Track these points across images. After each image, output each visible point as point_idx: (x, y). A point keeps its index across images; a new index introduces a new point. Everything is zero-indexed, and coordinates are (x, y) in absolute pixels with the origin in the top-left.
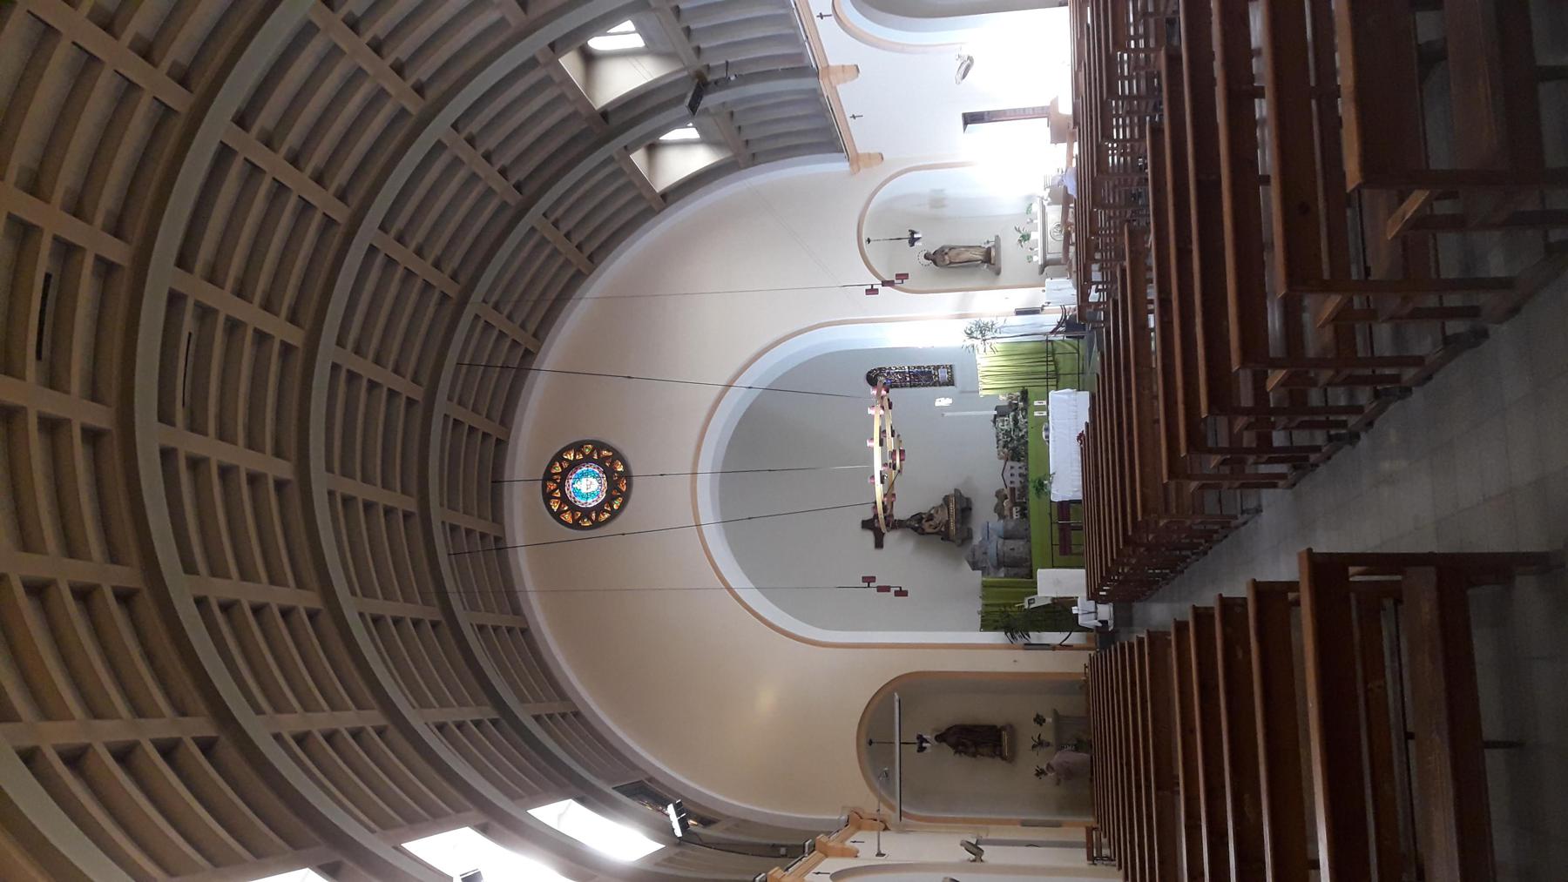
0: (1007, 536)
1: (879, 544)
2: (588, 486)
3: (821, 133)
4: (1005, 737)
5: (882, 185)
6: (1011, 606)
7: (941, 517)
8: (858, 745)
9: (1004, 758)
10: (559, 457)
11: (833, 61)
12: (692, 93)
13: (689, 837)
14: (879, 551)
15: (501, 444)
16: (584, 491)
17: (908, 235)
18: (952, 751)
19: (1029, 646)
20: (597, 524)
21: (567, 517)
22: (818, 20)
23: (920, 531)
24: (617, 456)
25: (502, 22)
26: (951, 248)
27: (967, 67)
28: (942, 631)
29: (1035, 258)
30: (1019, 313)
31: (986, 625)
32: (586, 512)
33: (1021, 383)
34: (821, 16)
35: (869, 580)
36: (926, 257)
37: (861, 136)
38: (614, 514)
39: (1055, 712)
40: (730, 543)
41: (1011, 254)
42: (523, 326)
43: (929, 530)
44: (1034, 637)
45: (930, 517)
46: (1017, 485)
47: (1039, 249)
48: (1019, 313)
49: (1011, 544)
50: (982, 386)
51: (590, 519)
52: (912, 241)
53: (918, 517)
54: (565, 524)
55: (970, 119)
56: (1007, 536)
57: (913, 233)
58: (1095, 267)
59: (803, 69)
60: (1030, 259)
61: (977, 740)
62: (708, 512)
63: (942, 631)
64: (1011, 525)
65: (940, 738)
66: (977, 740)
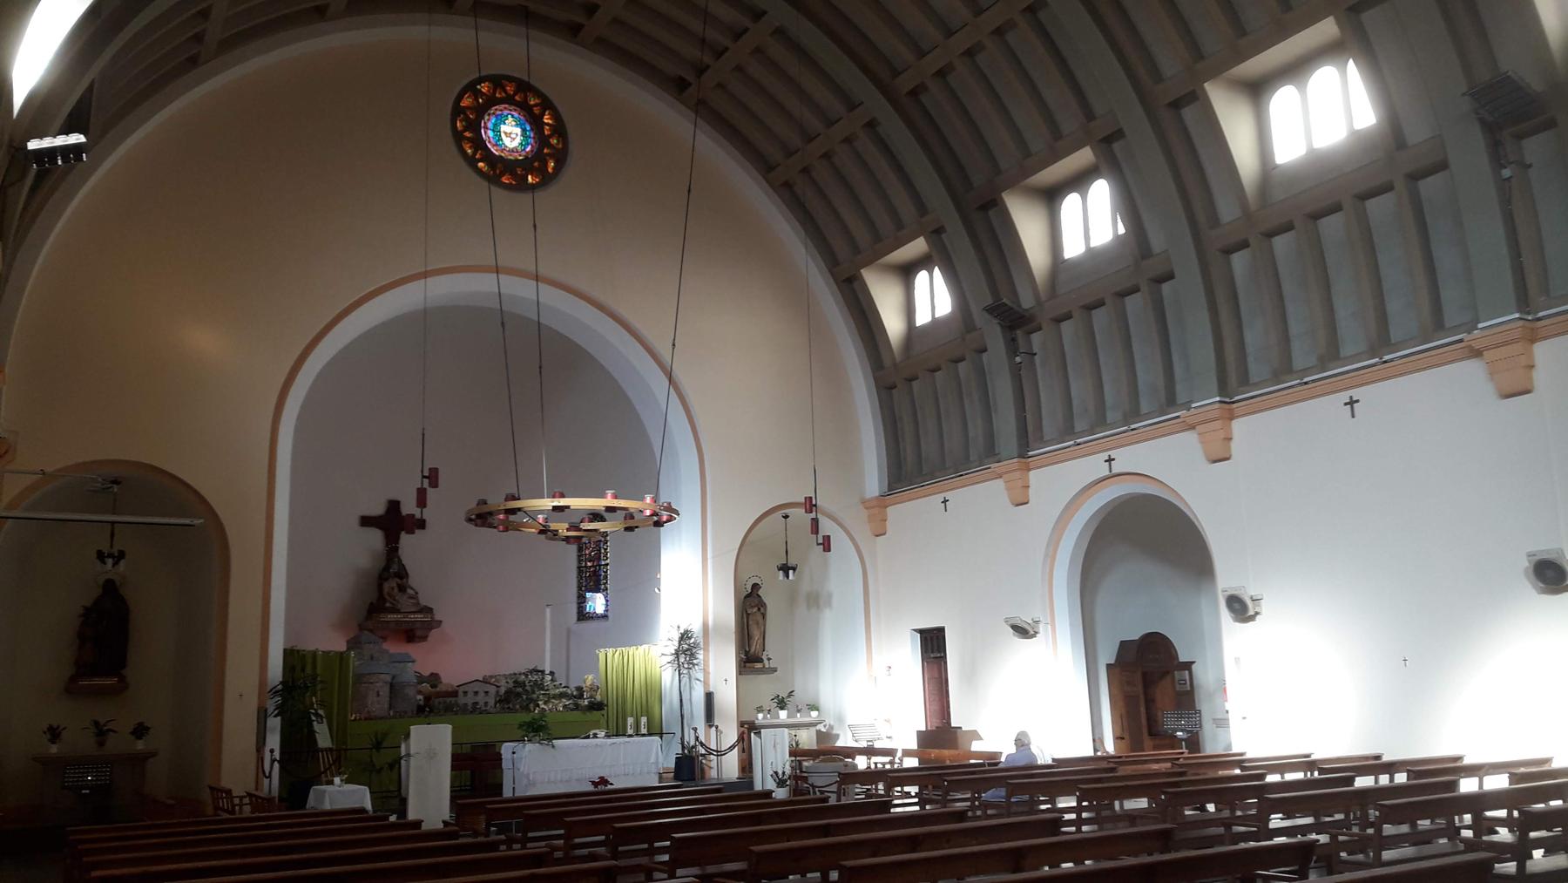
1: (366, 521)
2: (510, 135)
3: (914, 466)
5: (852, 539)
6: (314, 694)
7: (404, 602)
8: (101, 463)
9: (73, 679)
10: (547, 104)
12: (1007, 307)
13: (19, 153)
14: (355, 522)
15: (573, 31)
16: (503, 128)
17: (791, 563)
18: (88, 602)
19: (262, 715)
20: (458, 137)
21: (467, 101)
22: (1105, 456)
23: (383, 576)
24: (546, 180)
26: (764, 615)
27: (1022, 631)
28: (282, 599)
29: (760, 716)
30: (709, 697)
31: (290, 654)
32: (475, 126)
36: (755, 587)
37: (917, 512)
39: (153, 754)
40: (384, 324)
41: (765, 688)
43: (386, 586)
44: (275, 723)
45: (402, 589)
46: (462, 700)
48: (709, 697)
50: (610, 651)
52: (785, 569)
53: (402, 574)
54: (460, 97)
55: (933, 643)
57: (794, 569)
58: (1002, 792)
59: (1027, 443)
60: (760, 709)
61: (103, 640)
63: (282, 599)
64: (411, 692)
65: (110, 589)
66: (103, 640)
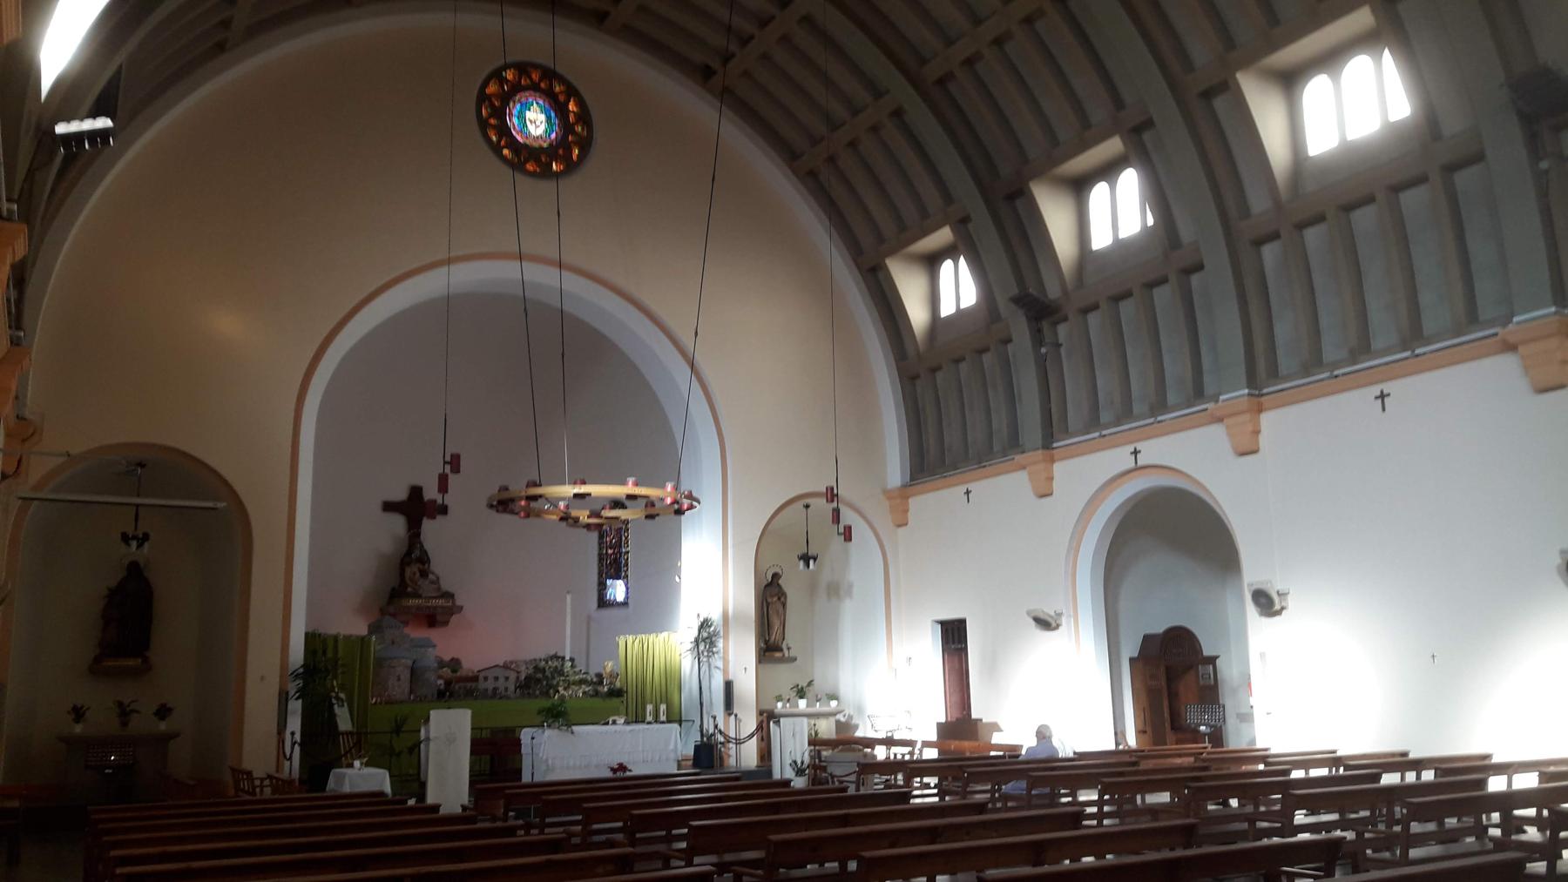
0: (415, 673)
1: (389, 507)
3: (935, 457)
4: (131, 662)
10: (572, 92)
11: (1058, 468)
12: (1034, 299)
16: (530, 115)
18: (113, 583)
19: (284, 698)
20: (483, 125)
21: (492, 88)
24: (571, 167)
25: (1188, 65)
26: (784, 605)
29: (780, 705)
30: (729, 686)
31: (311, 638)
33: (631, 690)
34: (1136, 452)
35: (455, 463)
36: (776, 576)
37: (938, 503)
38: (496, 149)
41: (784, 676)
42: (746, 74)
43: (408, 572)
44: (296, 706)
45: (424, 574)
46: (482, 685)
47: (789, 709)
48: (729, 686)
49: (406, 676)
51: (490, 116)
52: (806, 558)
53: (424, 559)
54: (485, 84)
55: (954, 635)
56: (415, 673)
59: (1052, 433)
60: (779, 698)
61: (127, 622)
62: (467, 276)
64: (431, 676)
66: (127, 622)
